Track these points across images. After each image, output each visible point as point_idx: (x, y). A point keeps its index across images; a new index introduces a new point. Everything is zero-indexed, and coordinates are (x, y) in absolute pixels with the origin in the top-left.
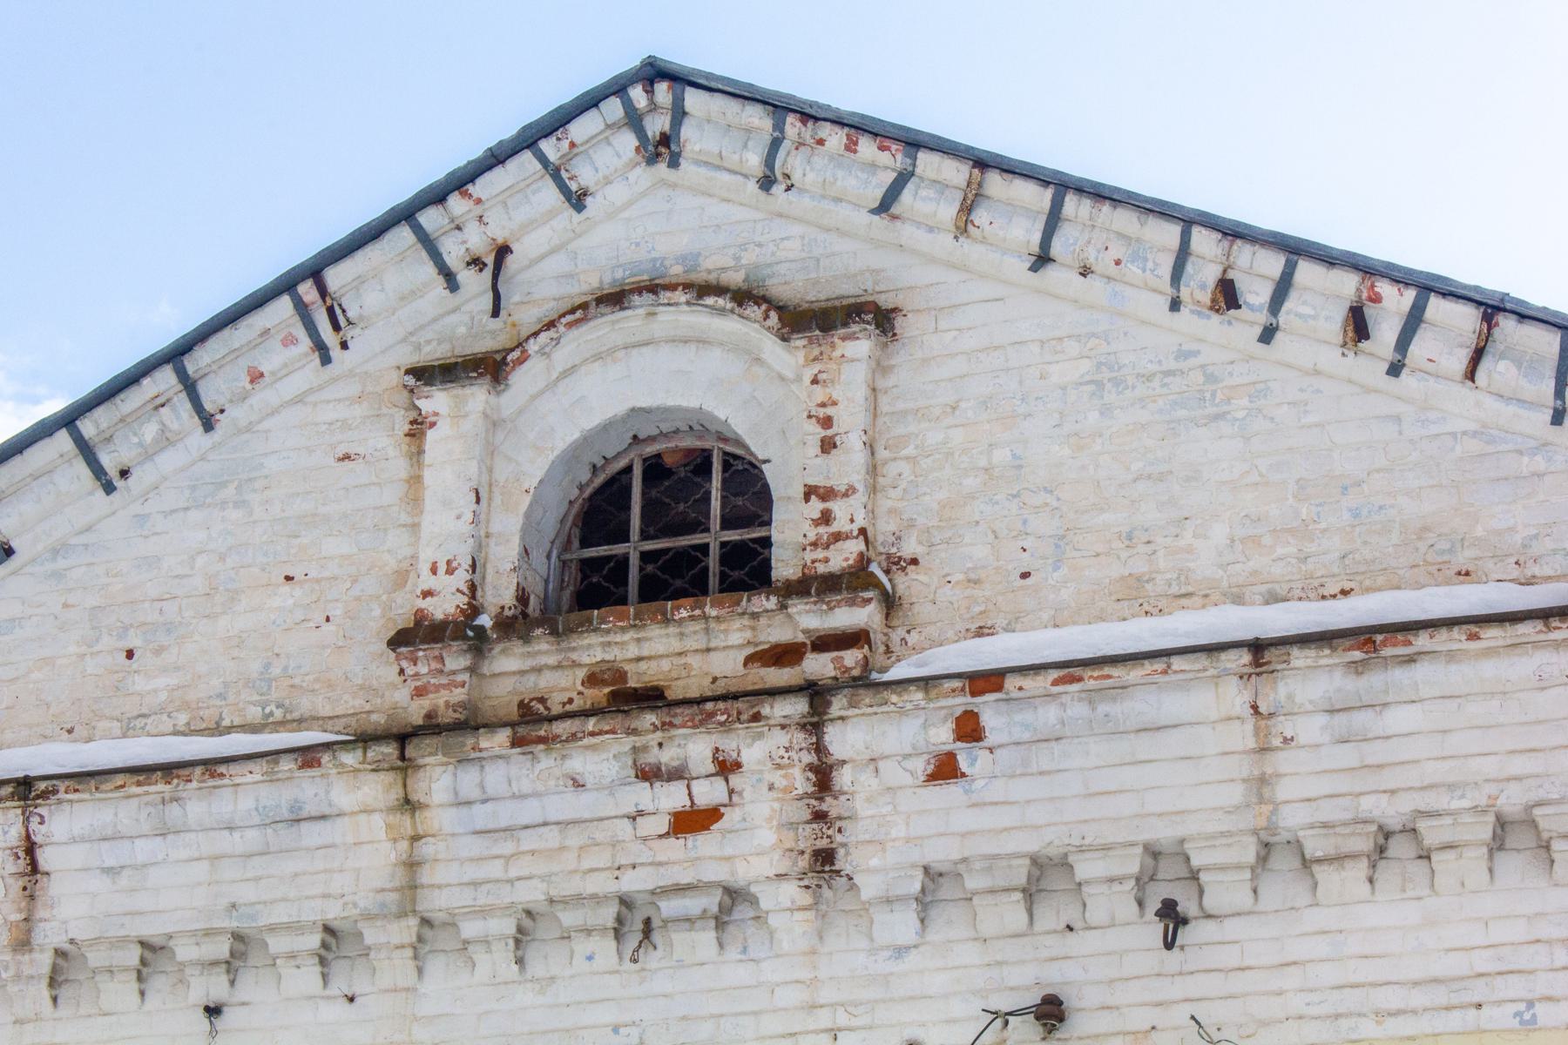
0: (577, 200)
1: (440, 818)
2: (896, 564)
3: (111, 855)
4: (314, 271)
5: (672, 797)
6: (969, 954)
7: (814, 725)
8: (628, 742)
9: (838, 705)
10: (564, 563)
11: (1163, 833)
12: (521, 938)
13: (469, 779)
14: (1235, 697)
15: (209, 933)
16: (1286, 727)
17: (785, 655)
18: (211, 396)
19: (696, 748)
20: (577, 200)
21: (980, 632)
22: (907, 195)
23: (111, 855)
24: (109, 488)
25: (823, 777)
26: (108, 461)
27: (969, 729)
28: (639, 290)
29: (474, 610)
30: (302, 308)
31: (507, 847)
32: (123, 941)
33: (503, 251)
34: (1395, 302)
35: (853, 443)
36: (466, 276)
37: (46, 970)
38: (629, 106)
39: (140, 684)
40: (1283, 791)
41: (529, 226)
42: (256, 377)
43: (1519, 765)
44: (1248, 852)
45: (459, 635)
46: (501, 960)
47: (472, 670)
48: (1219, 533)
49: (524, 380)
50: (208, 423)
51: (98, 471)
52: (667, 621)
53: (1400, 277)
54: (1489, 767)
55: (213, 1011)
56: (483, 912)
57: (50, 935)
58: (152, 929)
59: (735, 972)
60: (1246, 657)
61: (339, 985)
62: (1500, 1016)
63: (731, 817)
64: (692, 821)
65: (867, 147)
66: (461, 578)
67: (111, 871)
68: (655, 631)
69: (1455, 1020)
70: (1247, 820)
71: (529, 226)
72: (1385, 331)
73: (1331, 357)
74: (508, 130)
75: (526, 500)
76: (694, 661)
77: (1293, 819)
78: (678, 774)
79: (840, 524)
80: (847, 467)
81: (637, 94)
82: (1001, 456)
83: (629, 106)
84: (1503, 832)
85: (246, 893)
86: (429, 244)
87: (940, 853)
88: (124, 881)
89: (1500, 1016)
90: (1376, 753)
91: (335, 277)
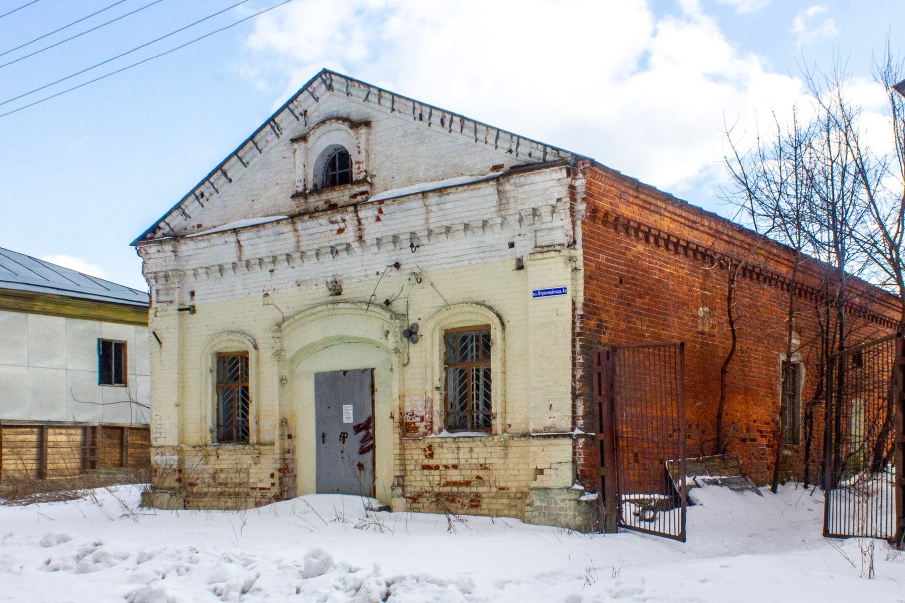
0: (317, 99)
1: (301, 232)
2: (372, 176)
3: (252, 242)
4: (272, 119)
5: (336, 227)
6: (386, 254)
7: (356, 212)
8: (327, 217)
9: (359, 208)
10: (327, 176)
11: (412, 230)
12: (317, 255)
13: (304, 225)
14: (421, 203)
15: (269, 257)
16: (430, 208)
17: (354, 196)
18: (260, 146)
19: (338, 217)
20: (317, 99)
21: (386, 190)
22: (370, 97)
23: (252, 242)
24: (246, 166)
25: (359, 221)
26: (244, 161)
27: (380, 211)
28: (327, 120)
29: (305, 190)
30: (272, 127)
31: (312, 238)
32: (255, 259)
33: (306, 112)
34: (448, 117)
35: (363, 151)
36: (300, 117)
37: (245, 265)
38: (322, 78)
39: (255, 207)
40: (431, 220)
41: (309, 106)
42: (267, 142)
43: (468, 214)
44: (426, 233)
45: (302, 196)
46: (314, 259)
47: (305, 202)
48: (423, 167)
49: (311, 140)
50: (261, 152)
51: (243, 163)
52: (335, 191)
53: (449, 113)
54: (462, 214)
55: (272, 271)
56: (310, 250)
57: (244, 258)
58: (260, 256)
59: (351, 260)
60: (421, 195)
61: (291, 265)
62: (466, 263)
63: (346, 230)
64: (341, 231)
65: (362, 87)
66: (303, 182)
67: (252, 245)
68: (334, 193)
69: (459, 264)
70: (425, 227)
71: (309, 106)
72: (447, 123)
73: (440, 129)
74: (301, 87)
75: (313, 166)
76: (341, 198)
77: (432, 226)
78: (336, 222)
79: (361, 169)
80: (362, 157)
81: (323, 76)
82: (389, 152)
83: (322, 78)
84: (466, 227)
85: (273, 249)
86: (292, 111)
87: (379, 235)
88: (255, 247)
89: (466, 263)
90: (446, 212)
91: (277, 120)
